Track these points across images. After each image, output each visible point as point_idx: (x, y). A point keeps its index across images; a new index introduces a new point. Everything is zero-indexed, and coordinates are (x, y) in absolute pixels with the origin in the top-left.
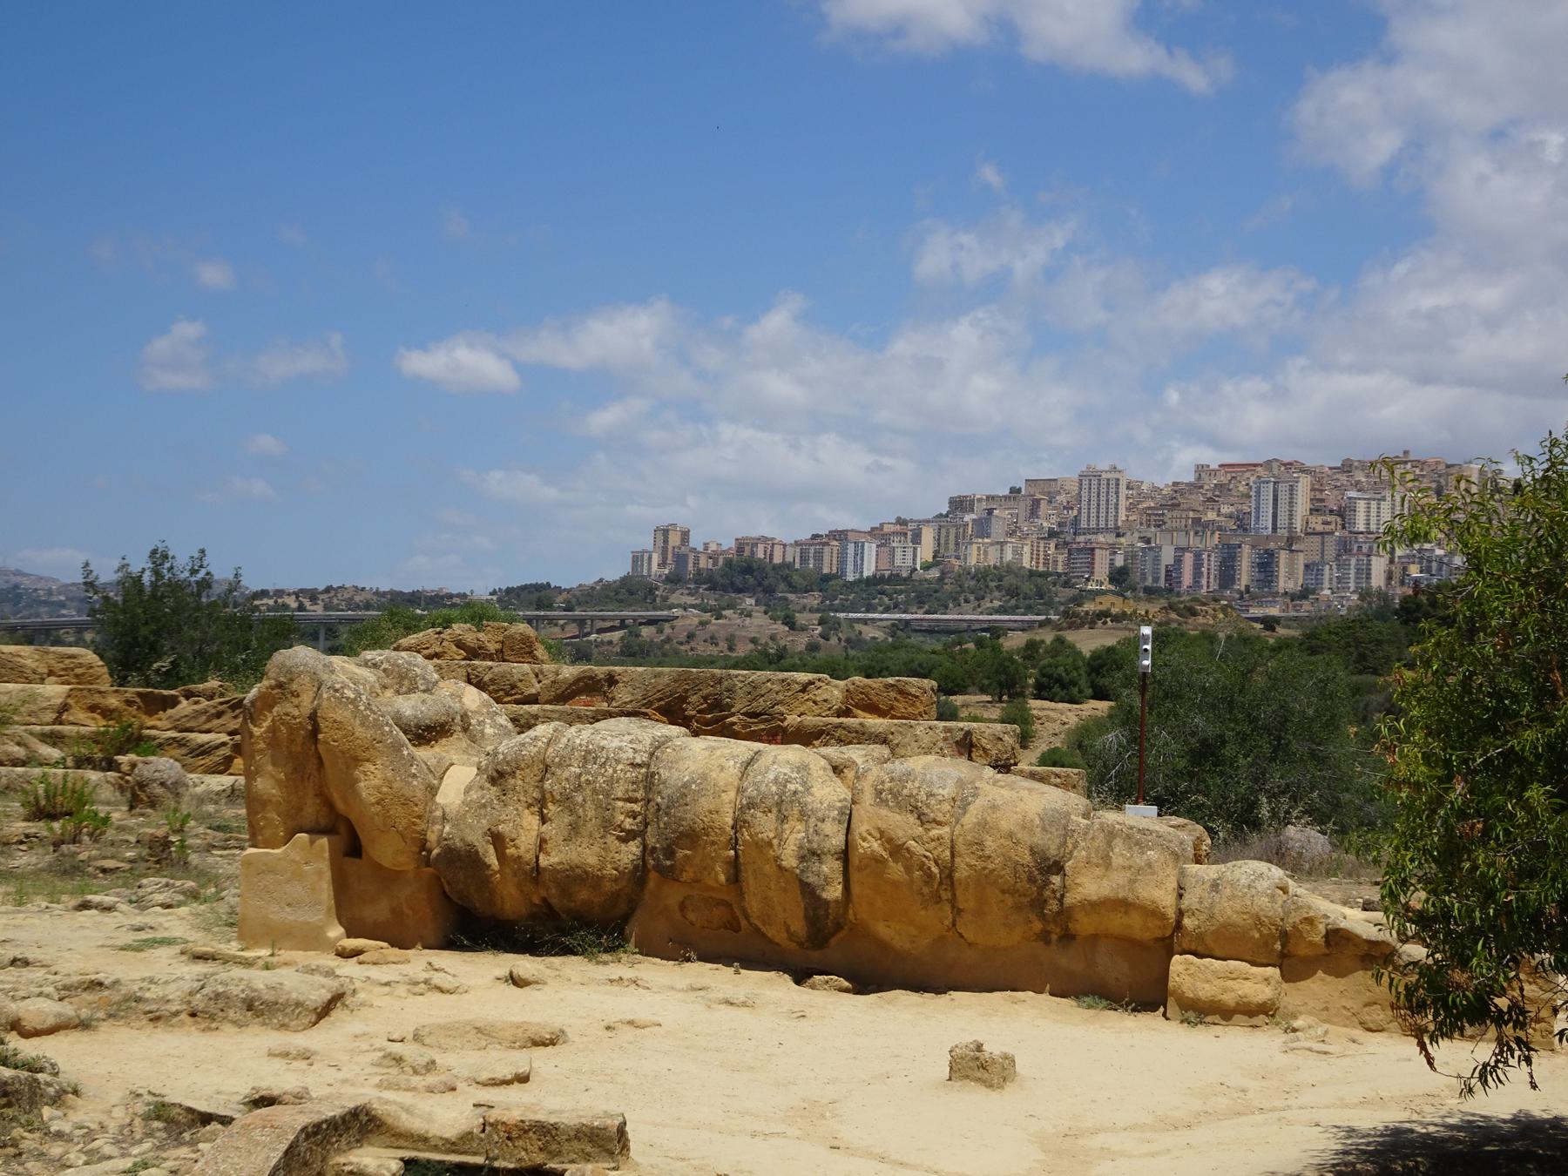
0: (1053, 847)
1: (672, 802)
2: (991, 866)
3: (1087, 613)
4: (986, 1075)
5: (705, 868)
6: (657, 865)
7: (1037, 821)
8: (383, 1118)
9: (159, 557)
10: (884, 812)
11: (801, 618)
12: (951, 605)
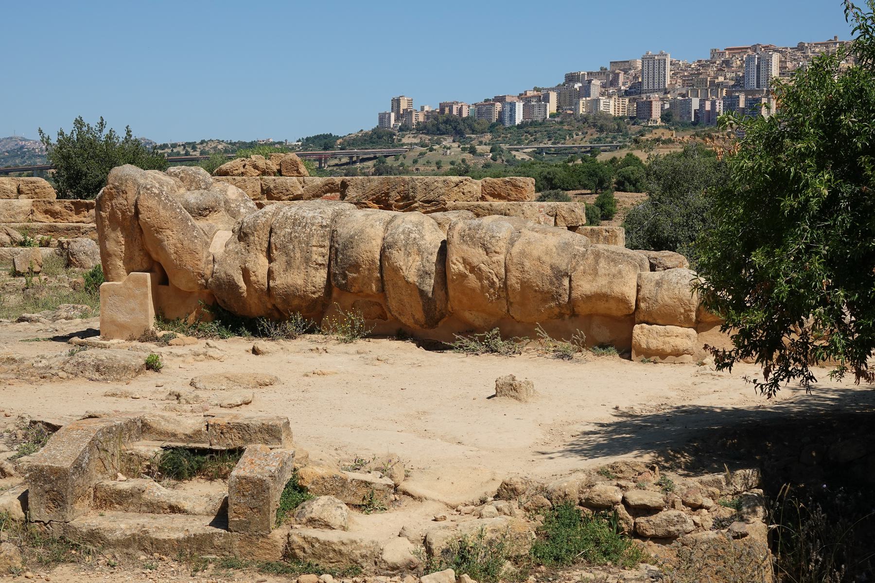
0: (564, 264)
1: (345, 247)
2: (528, 277)
3: (647, 140)
4: (517, 394)
5: (365, 284)
6: (337, 283)
7: (554, 250)
8: (151, 424)
9: (79, 123)
10: (465, 247)
11: (480, 149)
12: (568, 138)
